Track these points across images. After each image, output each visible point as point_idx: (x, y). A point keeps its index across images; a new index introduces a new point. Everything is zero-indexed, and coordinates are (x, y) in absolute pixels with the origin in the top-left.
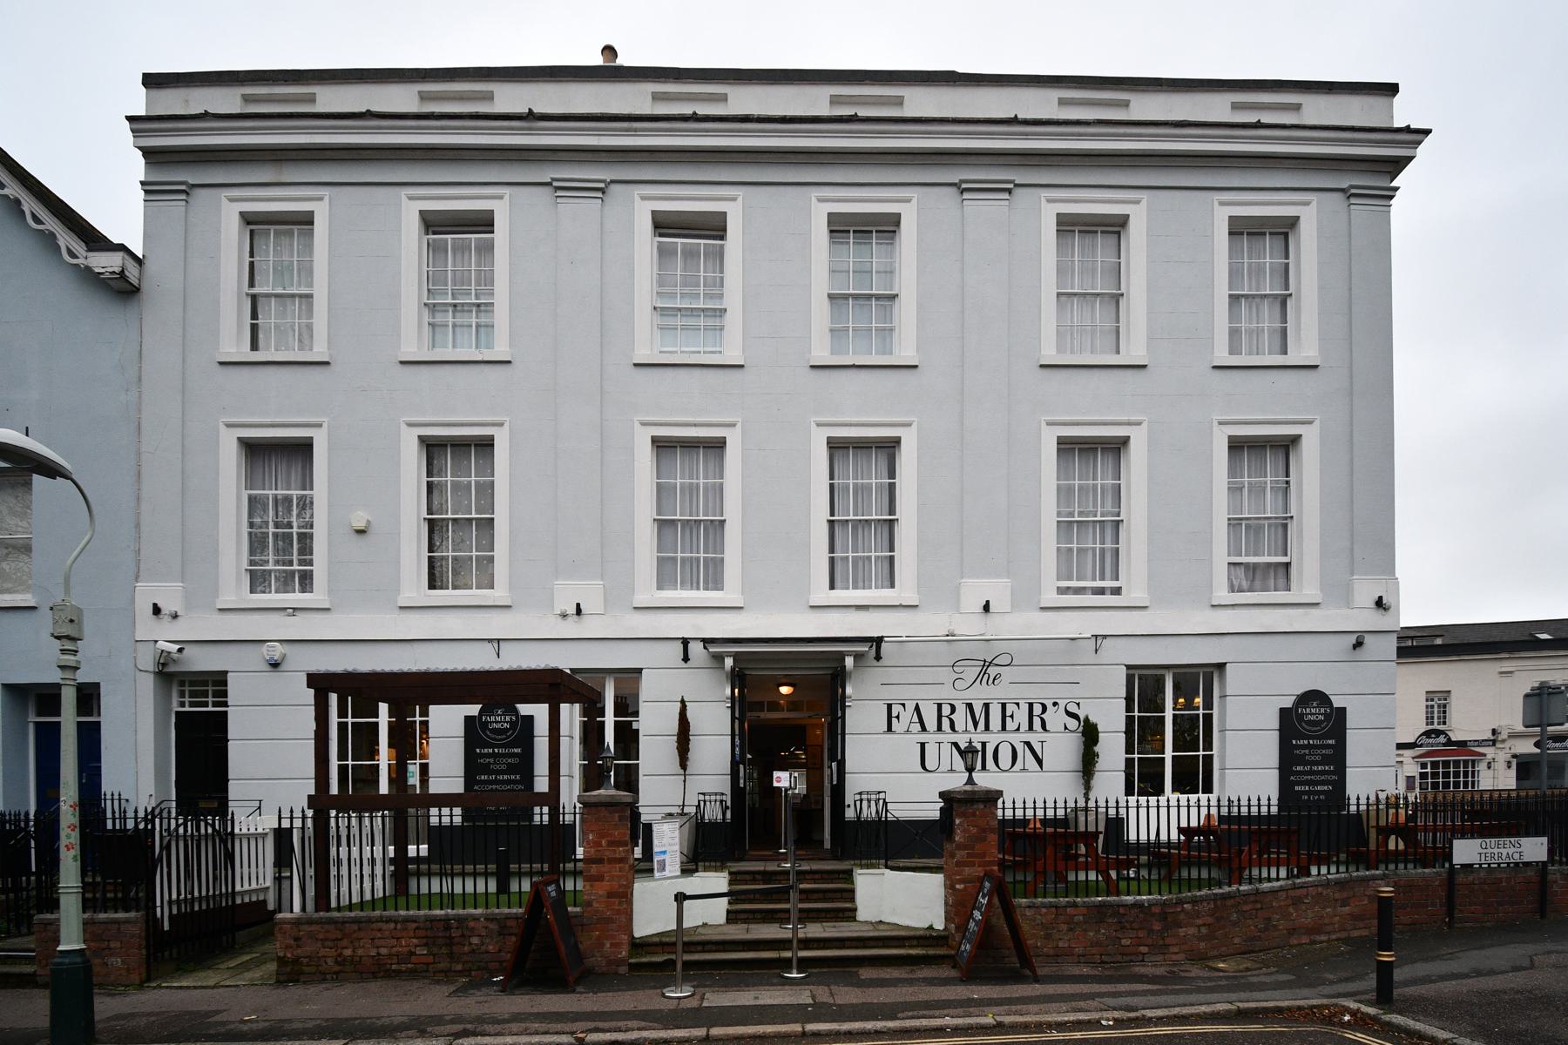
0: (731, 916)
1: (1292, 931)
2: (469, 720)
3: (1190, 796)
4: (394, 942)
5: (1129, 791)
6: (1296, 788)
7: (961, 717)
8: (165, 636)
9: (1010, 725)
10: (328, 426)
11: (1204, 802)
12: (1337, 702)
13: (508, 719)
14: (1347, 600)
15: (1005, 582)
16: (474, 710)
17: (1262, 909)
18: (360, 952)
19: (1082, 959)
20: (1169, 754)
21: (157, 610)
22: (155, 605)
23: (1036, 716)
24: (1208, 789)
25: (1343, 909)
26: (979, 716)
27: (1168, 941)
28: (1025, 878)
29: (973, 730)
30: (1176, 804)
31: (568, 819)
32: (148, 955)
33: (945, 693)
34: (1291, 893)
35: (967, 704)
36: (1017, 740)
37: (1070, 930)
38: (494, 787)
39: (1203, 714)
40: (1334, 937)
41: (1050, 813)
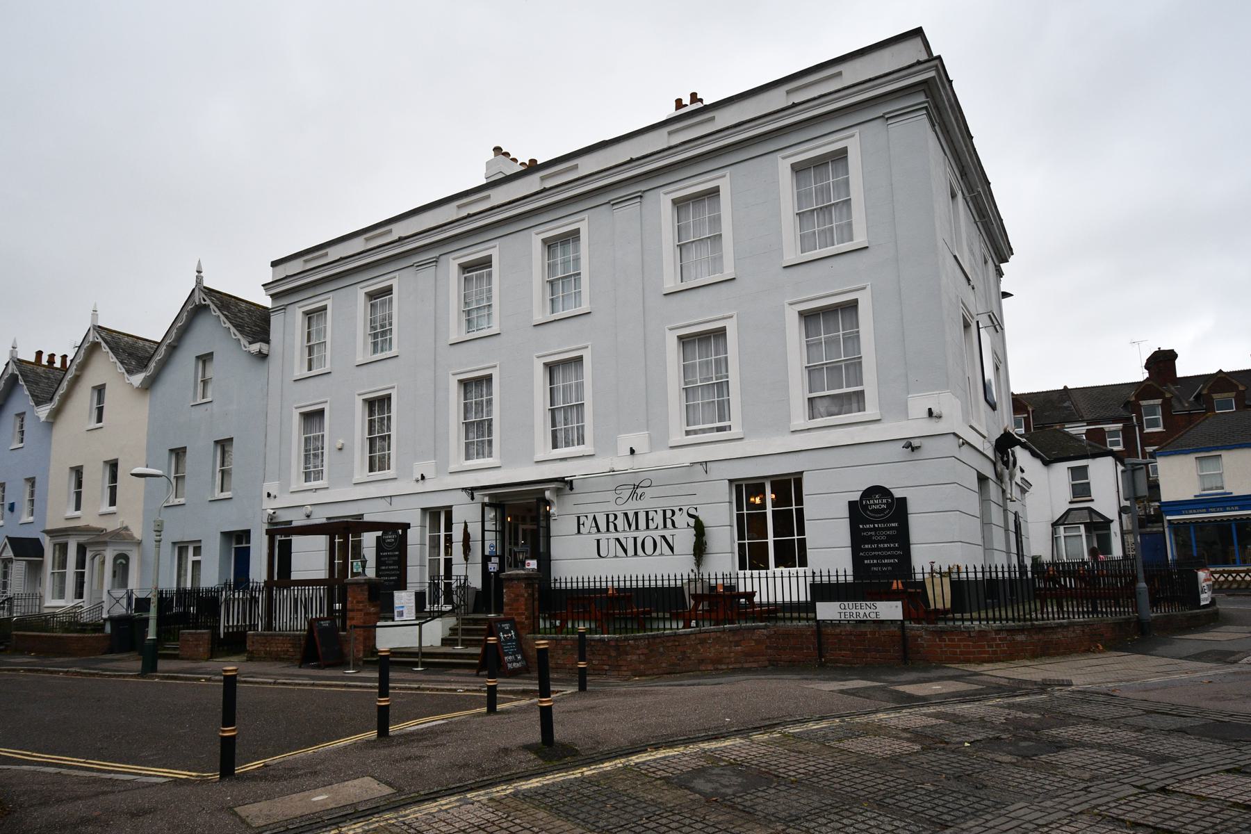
0: (444, 642)
1: (701, 661)
2: (378, 537)
3: (790, 569)
4: (282, 645)
5: (742, 567)
6: (866, 562)
7: (621, 522)
8: (269, 506)
9: (652, 525)
10: (871, 287)
11: (801, 574)
12: (897, 494)
13: (884, 501)
14: (904, 412)
15: (644, 434)
16: (380, 533)
17: (679, 645)
18: (272, 649)
19: (571, 671)
20: (771, 539)
21: (269, 495)
22: (631, 448)
23: (668, 519)
24: (803, 563)
25: (737, 648)
26: (632, 521)
27: (620, 663)
28: (671, 626)
29: (628, 530)
30: (648, 579)
31: (919, 577)
32: (212, 648)
33: (611, 507)
34: (698, 636)
35: (624, 513)
36: (656, 534)
37: (564, 653)
38: (877, 553)
39: (796, 509)
40: (731, 667)
41: (569, 585)
